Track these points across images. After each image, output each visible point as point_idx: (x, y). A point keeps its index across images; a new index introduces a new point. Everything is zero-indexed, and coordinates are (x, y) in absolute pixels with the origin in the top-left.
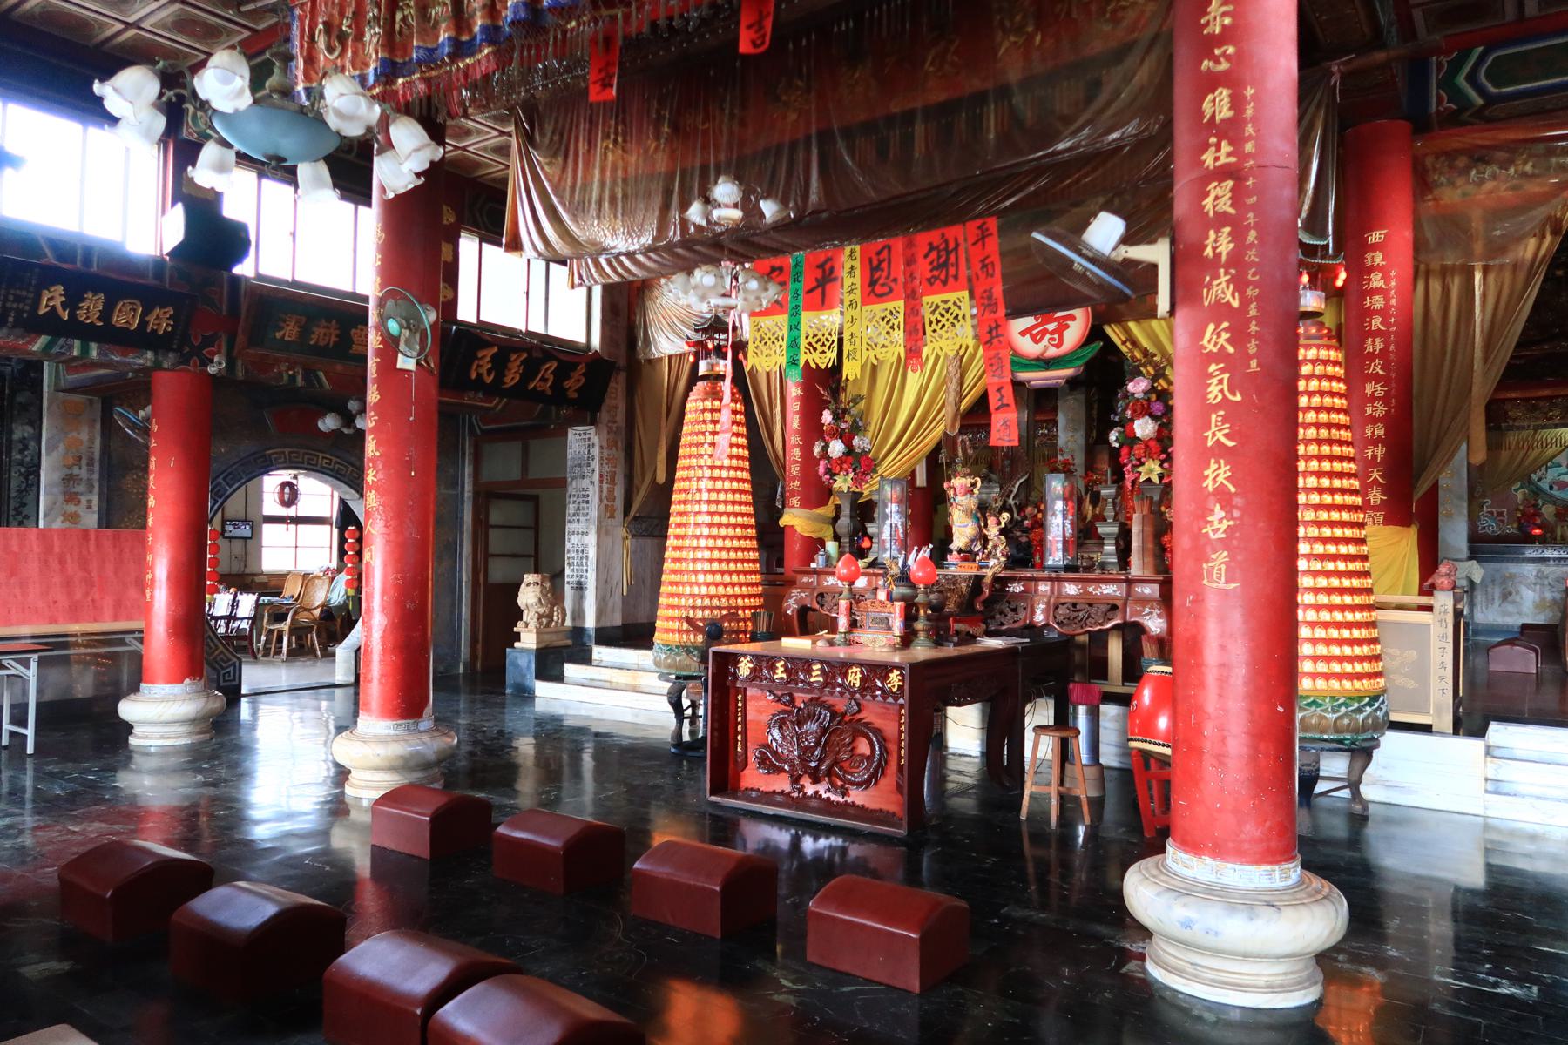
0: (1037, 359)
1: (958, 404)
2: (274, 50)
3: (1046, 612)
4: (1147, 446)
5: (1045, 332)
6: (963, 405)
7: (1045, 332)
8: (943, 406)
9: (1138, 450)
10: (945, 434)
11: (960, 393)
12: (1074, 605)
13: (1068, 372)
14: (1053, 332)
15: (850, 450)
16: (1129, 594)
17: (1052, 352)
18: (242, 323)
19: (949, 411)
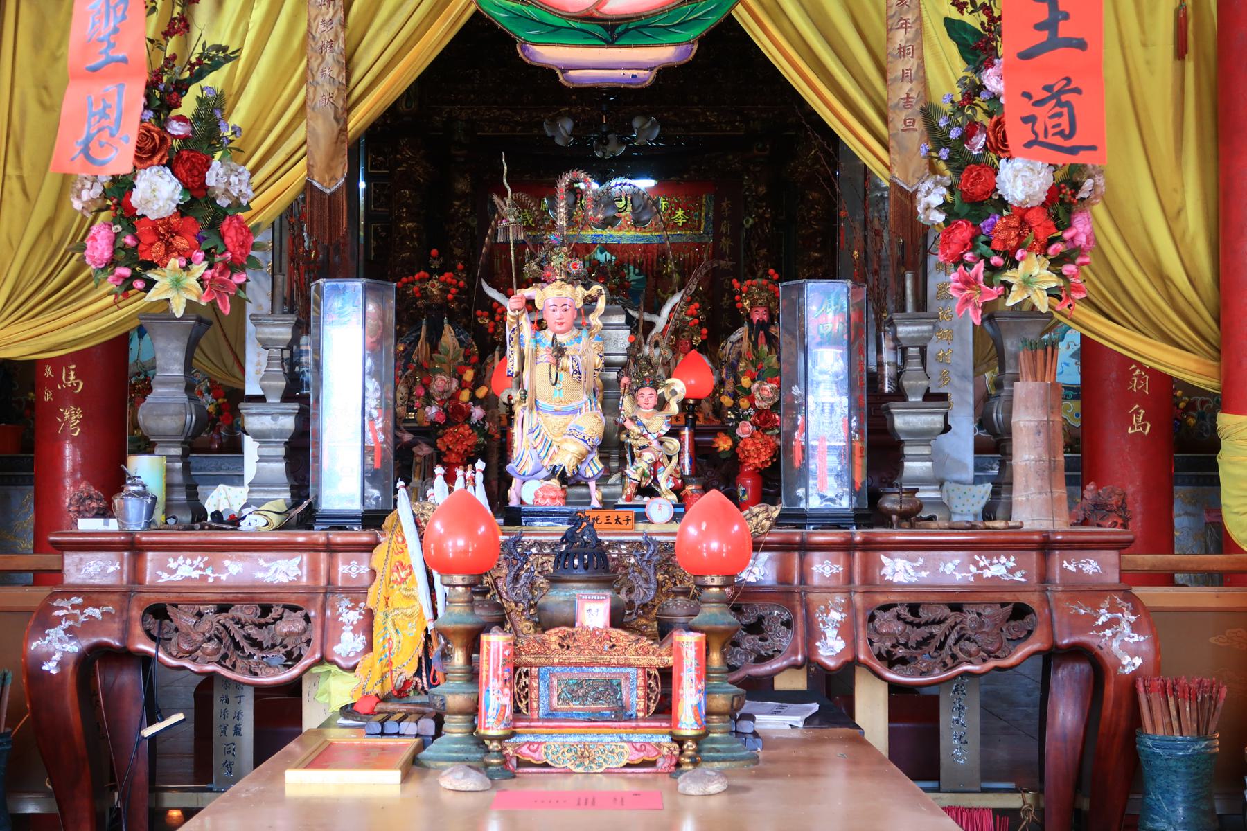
0: (587, 18)
1: (341, 118)
2: (105, 609)
3: (847, 631)
4: (1023, 222)
6: (358, 119)
9: (999, 226)
10: (308, 186)
11: (346, 86)
12: (914, 609)
13: (663, 54)
15: (197, 195)
16: (1044, 578)
18: (1217, 714)
19: (321, 127)
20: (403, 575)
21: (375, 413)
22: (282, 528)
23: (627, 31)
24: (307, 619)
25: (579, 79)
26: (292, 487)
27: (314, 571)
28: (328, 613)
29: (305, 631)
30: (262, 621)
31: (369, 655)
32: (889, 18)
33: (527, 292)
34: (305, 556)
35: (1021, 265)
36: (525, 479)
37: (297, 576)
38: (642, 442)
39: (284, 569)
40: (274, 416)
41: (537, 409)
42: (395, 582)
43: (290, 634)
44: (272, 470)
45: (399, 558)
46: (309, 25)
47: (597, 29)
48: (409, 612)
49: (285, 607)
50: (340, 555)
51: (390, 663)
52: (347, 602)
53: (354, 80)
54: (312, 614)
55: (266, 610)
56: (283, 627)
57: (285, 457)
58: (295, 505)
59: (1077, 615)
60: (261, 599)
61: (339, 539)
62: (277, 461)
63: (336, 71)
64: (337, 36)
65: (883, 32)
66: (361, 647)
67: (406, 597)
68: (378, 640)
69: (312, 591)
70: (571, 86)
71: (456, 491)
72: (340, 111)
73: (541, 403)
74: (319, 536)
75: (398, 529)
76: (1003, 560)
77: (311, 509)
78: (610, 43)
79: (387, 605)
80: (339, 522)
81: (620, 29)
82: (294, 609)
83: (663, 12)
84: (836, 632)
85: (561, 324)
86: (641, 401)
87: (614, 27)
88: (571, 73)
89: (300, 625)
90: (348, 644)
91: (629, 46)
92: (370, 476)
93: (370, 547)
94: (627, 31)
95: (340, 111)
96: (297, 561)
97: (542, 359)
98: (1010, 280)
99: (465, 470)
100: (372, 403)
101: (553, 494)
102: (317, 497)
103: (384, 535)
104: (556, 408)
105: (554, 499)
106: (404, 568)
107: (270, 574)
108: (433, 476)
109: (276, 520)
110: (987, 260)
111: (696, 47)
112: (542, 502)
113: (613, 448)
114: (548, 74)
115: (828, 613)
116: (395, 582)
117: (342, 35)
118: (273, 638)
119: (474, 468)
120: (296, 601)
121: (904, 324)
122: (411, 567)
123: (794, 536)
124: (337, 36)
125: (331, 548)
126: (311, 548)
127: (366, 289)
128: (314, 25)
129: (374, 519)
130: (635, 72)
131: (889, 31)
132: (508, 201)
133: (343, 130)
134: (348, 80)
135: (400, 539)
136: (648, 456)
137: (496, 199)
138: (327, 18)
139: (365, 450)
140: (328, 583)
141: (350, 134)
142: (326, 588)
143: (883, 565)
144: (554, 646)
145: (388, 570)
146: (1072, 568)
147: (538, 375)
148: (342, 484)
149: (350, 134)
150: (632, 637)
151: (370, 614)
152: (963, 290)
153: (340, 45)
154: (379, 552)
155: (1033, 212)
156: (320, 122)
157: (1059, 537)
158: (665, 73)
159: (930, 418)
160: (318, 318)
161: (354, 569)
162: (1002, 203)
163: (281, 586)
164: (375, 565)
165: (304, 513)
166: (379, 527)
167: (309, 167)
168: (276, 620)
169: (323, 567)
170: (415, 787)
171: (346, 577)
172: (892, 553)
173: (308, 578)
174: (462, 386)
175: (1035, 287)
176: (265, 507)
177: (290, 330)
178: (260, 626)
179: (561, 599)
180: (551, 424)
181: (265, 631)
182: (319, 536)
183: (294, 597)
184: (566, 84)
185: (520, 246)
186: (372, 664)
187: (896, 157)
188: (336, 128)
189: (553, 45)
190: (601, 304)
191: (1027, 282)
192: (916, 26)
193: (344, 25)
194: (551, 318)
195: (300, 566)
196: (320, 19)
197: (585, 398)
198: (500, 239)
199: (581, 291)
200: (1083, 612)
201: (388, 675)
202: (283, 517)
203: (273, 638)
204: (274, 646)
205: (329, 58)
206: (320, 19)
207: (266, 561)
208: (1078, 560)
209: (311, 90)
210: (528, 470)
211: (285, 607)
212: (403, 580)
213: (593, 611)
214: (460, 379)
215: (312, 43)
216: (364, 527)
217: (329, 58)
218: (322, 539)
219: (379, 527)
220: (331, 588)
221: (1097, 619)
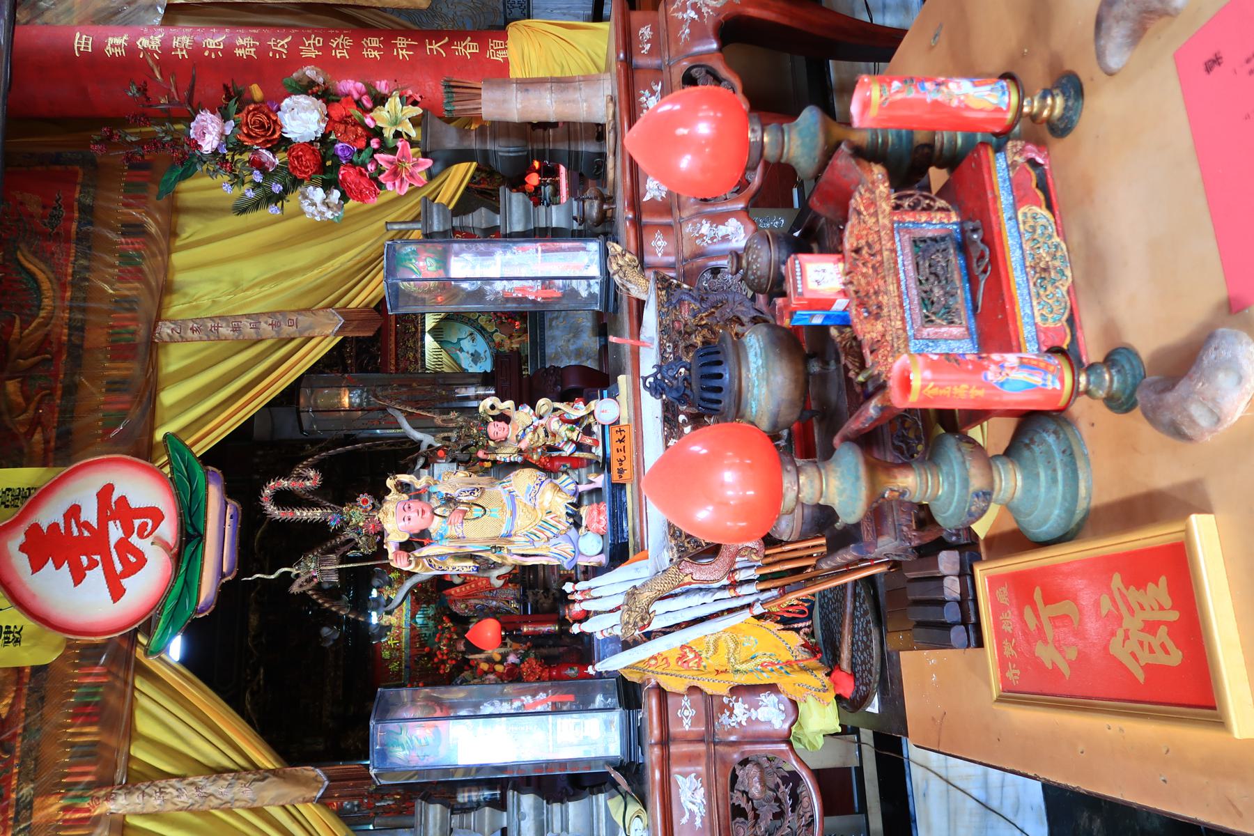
0: (177, 558)
5: (124, 546)
6: (265, 760)
7: (124, 546)
8: (258, 811)
10: (323, 801)
11: (237, 772)
13: (214, 495)
14: (128, 530)
17: (168, 530)
19: (271, 794)
20: (691, 656)
21: (517, 704)
22: (643, 801)
23: (192, 525)
24: (744, 762)
25: (232, 563)
26: (592, 793)
27: (691, 759)
28: (733, 738)
29: (758, 764)
30: (751, 815)
31: (781, 686)
32: (209, 340)
33: (391, 548)
34: (675, 769)
35: (380, 124)
36: (577, 552)
37: (697, 778)
38: (541, 431)
39: (689, 794)
40: (521, 817)
41: (510, 536)
42: (699, 665)
43: (762, 781)
44: (576, 816)
45: (672, 661)
46: (181, 810)
47: (190, 548)
48: (732, 645)
49: (732, 790)
50: (671, 730)
51: (788, 663)
52: (724, 719)
53: (231, 766)
54: (736, 757)
55: (738, 812)
56: (756, 790)
57: (562, 802)
58: (615, 785)
59: (690, 34)
60: (726, 818)
61: (656, 732)
62: (567, 811)
63: (222, 782)
64: (192, 784)
65: (223, 343)
66: (773, 698)
67: (715, 651)
68: (765, 679)
69: (712, 759)
70: (236, 569)
71: (601, 605)
72: (257, 776)
73: (503, 531)
74: (652, 755)
75: (641, 665)
76: (643, 99)
77: (621, 767)
78: (201, 537)
79: (726, 671)
80: (634, 736)
81: (191, 530)
82: (734, 778)
83: (178, 495)
84: (721, 227)
85: (423, 512)
86: (501, 435)
87: (188, 534)
88: (225, 570)
89: (751, 769)
90: (770, 713)
91: (206, 522)
92: (583, 706)
93: (662, 694)
94: (192, 525)
95: (257, 776)
96: (680, 779)
97: (459, 531)
98: (393, 132)
99: (574, 601)
100: (506, 708)
101: (595, 513)
102: (609, 762)
103: (649, 679)
104: (509, 515)
105: (599, 513)
106: (684, 655)
107: (695, 808)
108: (582, 633)
109: (634, 808)
110: (375, 151)
111: (210, 468)
112: (604, 523)
113: (549, 463)
114: (226, 591)
115: (703, 235)
116: (699, 665)
117: (191, 779)
118: (768, 801)
119: (572, 593)
120: (725, 776)
121: (432, 225)
122: (683, 647)
123: (687, 44)
124: (192, 784)
125: (666, 741)
126: (665, 763)
127: (382, 719)
128: (181, 805)
129: (628, 694)
130: (228, 516)
131: (219, 339)
132: (294, 571)
133: (274, 772)
134: (229, 771)
135: (653, 662)
136: (555, 425)
137: (295, 589)
138: (175, 793)
139: (556, 711)
140: (702, 741)
141: (278, 766)
142: (708, 744)
143: (653, 199)
144: (879, 326)
145: (687, 673)
146: (648, 47)
147: (475, 533)
148: (591, 736)
149: (278, 766)
150: (853, 219)
151: (737, 690)
152: (402, 180)
153: (199, 780)
154: (670, 684)
155: (333, 113)
156: (265, 794)
157: (622, 56)
158: (230, 492)
159: (514, 203)
160: (418, 772)
161: (686, 713)
162: (325, 136)
163: (708, 795)
164: (682, 688)
165: (627, 776)
166: (640, 686)
167: (305, 801)
168: (749, 799)
169: (686, 748)
170: (1214, 491)
171: (695, 721)
172: (641, 191)
173: (698, 765)
174: (493, 671)
175: (400, 115)
176: (619, 820)
177: (431, 806)
178: (757, 817)
179: (764, 390)
180: (523, 522)
181: (762, 811)
182: (652, 755)
183: (721, 780)
184: (234, 574)
185: (344, 559)
186: (791, 683)
187: (317, 331)
188: (272, 779)
189: (200, 586)
190: (405, 478)
191: (396, 122)
192: (217, 320)
193: (182, 778)
194: (417, 524)
195: (685, 775)
196: (176, 800)
197: (499, 488)
198: (335, 578)
199: (393, 497)
200: (687, 31)
201: (802, 664)
202: (629, 798)
203: (768, 801)
204: (777, 800)
205: (211, 789)
206: (176, 800)
207: (683, 815)
208: (640, 42)
209: (238, 804)
210: (569, 548)
211: (732, 790)
212: (698, 656)
213: (818, 277)
214: (486, 673)
215: (196, 806)
216: (639, 706)
217: (211, 789)
218: (656, 751)
219: (640, 686)
220: (709, 738)
221: (693, 19)
